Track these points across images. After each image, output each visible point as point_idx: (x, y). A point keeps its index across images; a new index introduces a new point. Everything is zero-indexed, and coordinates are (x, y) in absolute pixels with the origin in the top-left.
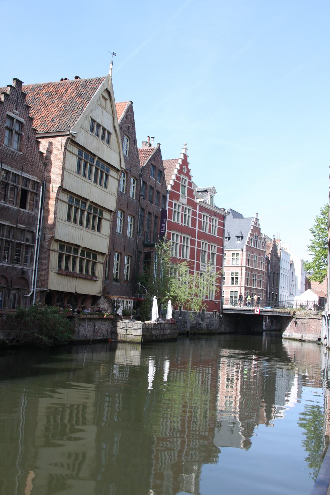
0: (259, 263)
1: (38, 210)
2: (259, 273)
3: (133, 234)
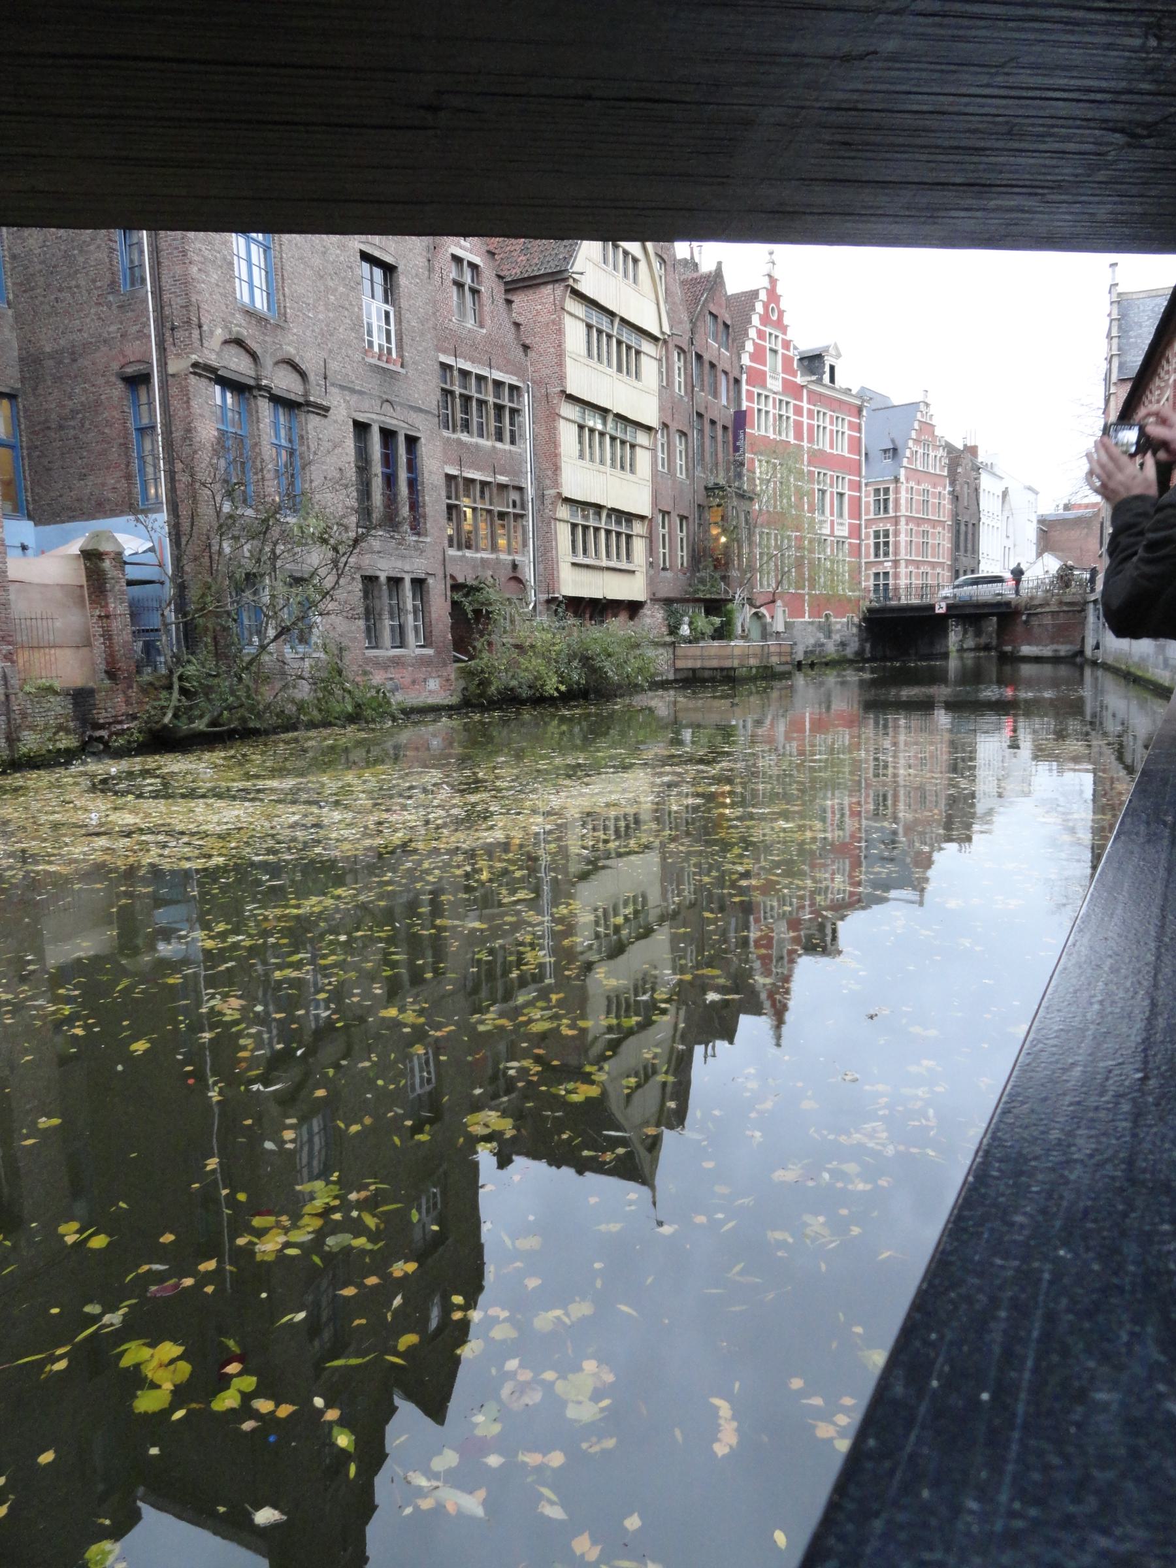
0: (934, 504)
1: (525, 443)
2: (934, 528)
3: (687, 470)
